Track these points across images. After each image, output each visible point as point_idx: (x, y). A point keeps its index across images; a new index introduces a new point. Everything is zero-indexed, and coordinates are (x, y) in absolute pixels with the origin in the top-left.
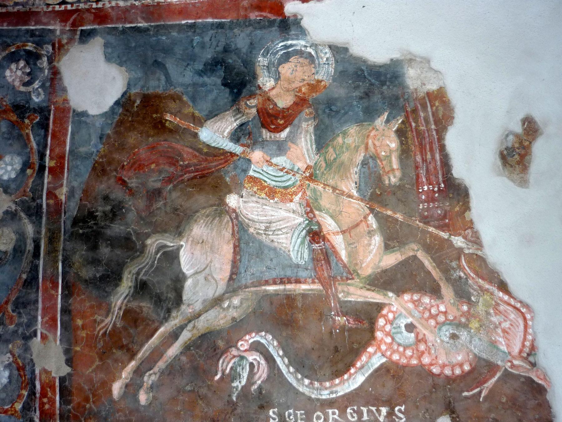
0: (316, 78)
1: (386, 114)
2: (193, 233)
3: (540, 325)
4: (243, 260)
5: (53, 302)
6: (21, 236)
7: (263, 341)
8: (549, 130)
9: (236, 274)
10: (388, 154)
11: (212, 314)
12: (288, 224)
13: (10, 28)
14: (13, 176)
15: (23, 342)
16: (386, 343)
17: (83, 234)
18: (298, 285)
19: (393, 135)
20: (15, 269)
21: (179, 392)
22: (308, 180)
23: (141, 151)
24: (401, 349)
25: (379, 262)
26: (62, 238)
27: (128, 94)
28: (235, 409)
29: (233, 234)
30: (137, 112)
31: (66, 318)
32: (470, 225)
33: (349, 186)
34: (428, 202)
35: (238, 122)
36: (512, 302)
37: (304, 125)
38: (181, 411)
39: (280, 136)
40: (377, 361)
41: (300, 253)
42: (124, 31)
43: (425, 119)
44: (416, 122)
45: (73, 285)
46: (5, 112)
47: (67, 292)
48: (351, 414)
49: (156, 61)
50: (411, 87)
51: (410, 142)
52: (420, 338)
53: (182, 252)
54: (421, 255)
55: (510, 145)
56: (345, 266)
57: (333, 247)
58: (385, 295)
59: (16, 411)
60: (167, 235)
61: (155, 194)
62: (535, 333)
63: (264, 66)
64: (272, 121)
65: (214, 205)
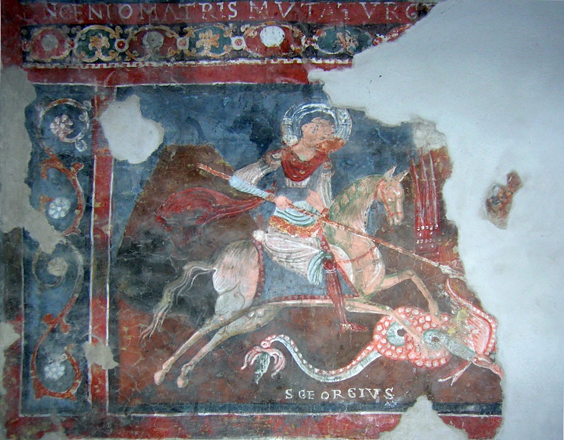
0: (335, 136)
1: (394, 168)
2: (225, 261)
3: (501, 333)
4: (267, 282)
5: (102, 315)
6: (73, 265)
7: (282, 341)
8: (528, 184)
9: (261, 292)
10: (394, 200)
11: (239, 322)
12: (306, 255)
13: (50, 84)
14: (63, 215)
15: (76, 345)
16: (381, 344)
17: (128, 262)
18: (313, 301)
19: (399, 185)
20: (68, 290)
21: (211, 378)
22: (325, 220)
23: (178, 195)
24: (393, 348)
25: (380, 284)
26: (109, 265)
27: (164, 147)
28: (258, 390)
29: (259, 262)
30: (173, 162)
31: (114, 326)
32: (456, 256)
33: (359, 225)
34: (424, 239)
35: (264, 172)
36: (483, 315)
37: (323, 175)
38: (213, 391)
39: (301, 184)
40: (374, 356)
41: (315, 277)
42: (158, 89)
43: (426, 174)
44: (420, 175)
45: (119, 302)
46: (52, 161)
47: (114, 307)
48: (351, 393)
49: (189, 118)
50: (418, 146)
51: (413, 191)
52: (409, 340)
53: (214, 276)
54: (415, 279)
55: (495, 195)
56: (352, 286)
57: (343, 272)
58: (383, 308)
59: (71, 395)
60: (201, 262)
61: (191, 230)
62: (497, 338)
63: (289, 125)
64: (294, 172)
65: (243, 239)
